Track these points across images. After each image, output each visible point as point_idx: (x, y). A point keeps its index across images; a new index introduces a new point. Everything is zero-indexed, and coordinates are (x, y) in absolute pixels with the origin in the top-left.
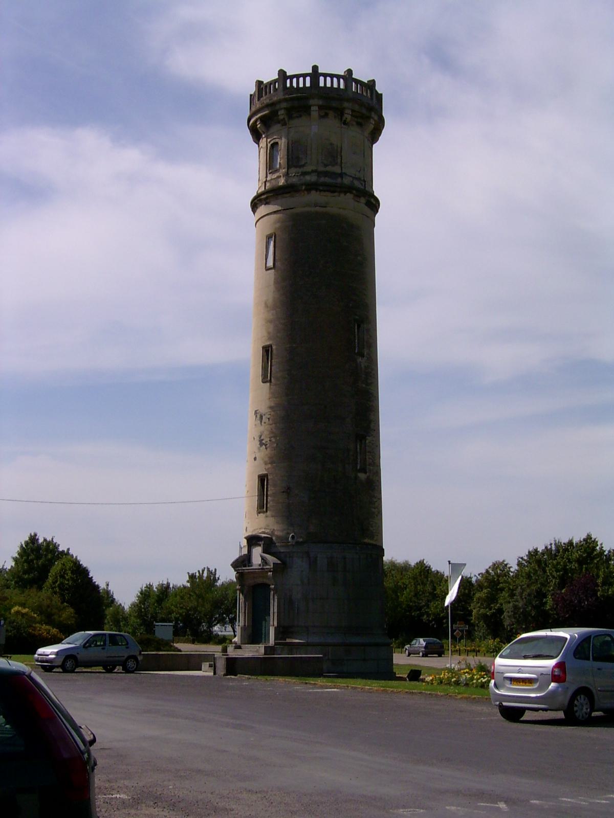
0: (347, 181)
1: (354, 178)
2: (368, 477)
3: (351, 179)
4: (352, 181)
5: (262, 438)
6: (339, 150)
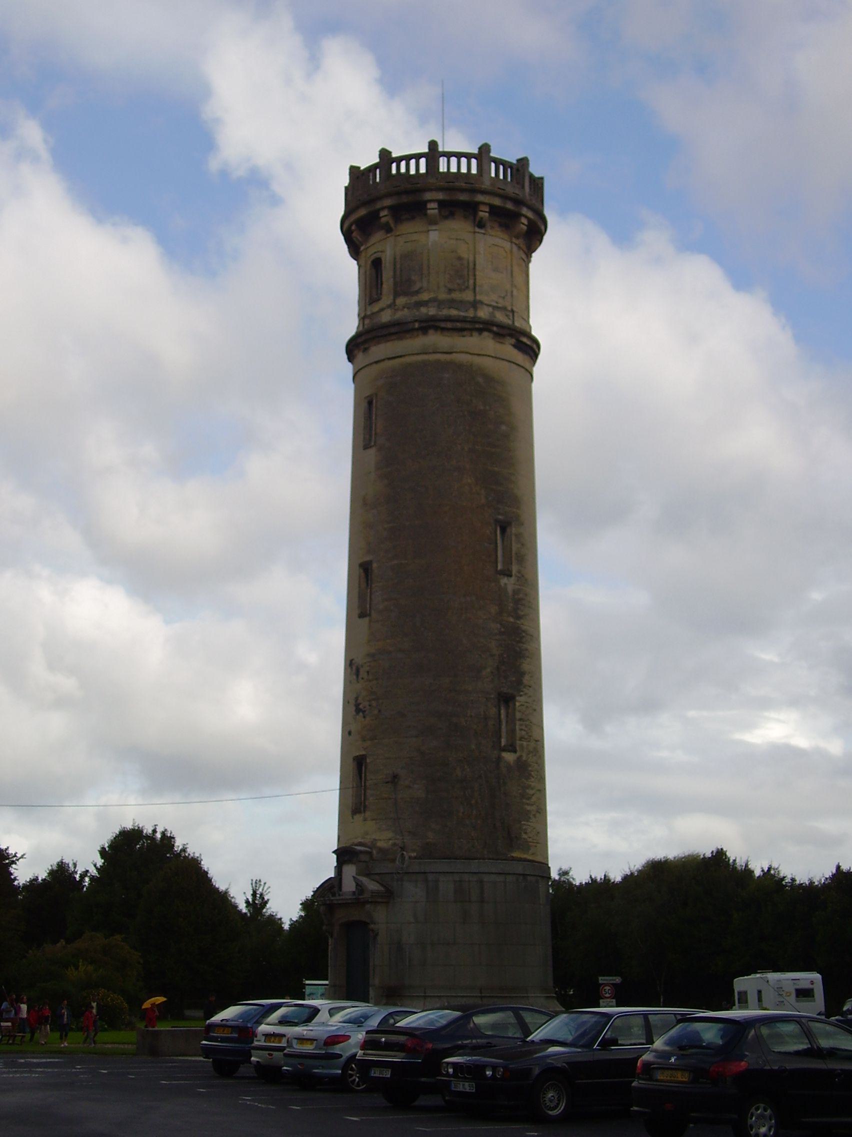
0: (483, 313)
1: (495, 308)
2: (519, 758)
3: (491, 309)
4: (493, 313)
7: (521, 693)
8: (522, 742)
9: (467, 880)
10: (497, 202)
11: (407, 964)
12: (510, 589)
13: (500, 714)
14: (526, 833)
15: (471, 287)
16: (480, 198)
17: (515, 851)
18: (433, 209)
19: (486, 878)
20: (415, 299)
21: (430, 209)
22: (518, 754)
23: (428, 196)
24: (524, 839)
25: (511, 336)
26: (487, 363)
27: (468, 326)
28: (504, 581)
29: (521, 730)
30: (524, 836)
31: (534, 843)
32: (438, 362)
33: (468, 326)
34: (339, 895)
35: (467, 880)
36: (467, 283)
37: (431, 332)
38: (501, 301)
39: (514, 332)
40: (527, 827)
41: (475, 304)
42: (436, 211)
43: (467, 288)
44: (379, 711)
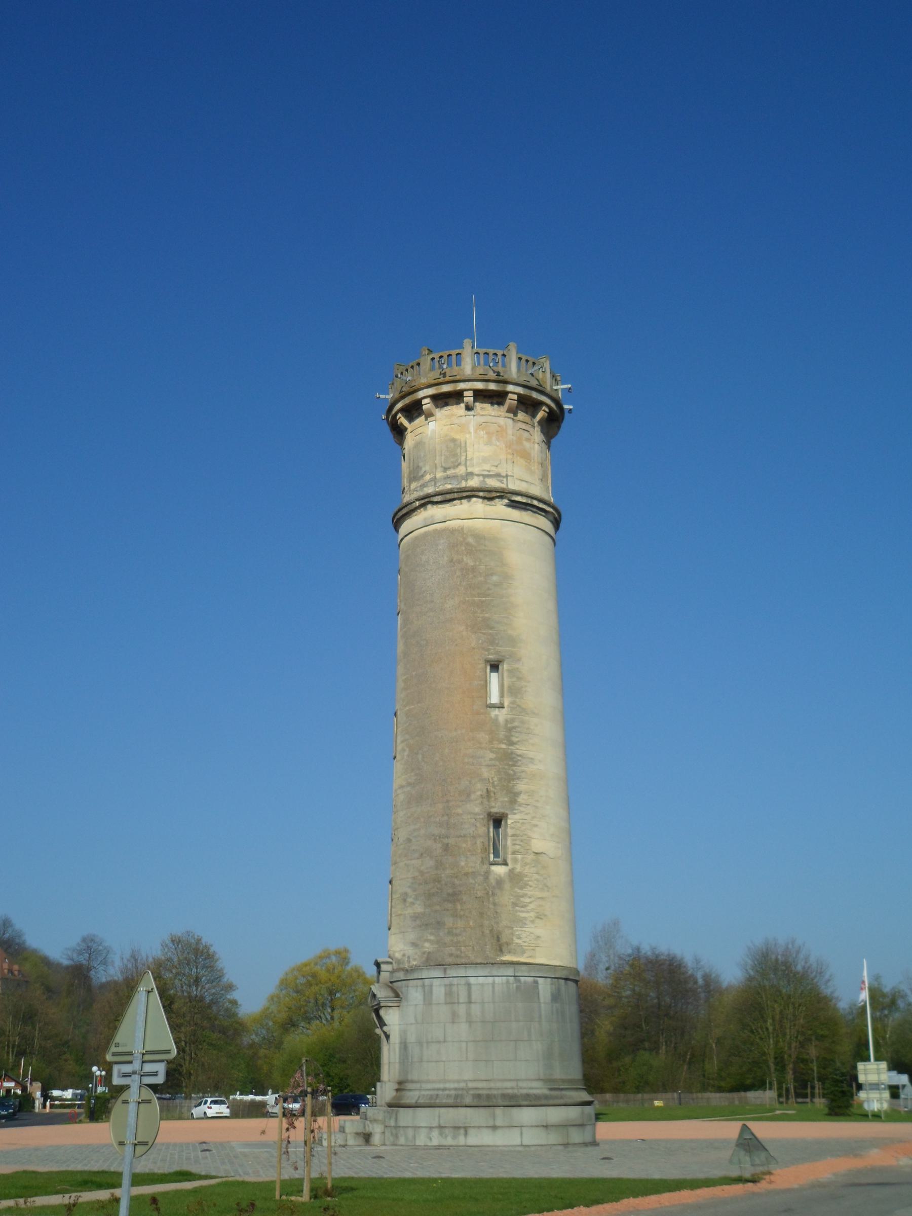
0: (474, 483)
1: (485, 476)
2: (512, 871)
3: (481, 478)
4: (484, 481)
7: (515, 811)
8: (515, 855)
9: (456, 983)
10: (480, 386)
11: (410, 1061)
12: (501, 719)
13: (489, 832)
14: (519, 938)
15: (463, 463)
16: (510, 388)
17: (506, 955)
18: (469, 397)
19: (472, 980)
20: (421, 482)
21: (425, 405)
22: (510, 866)
23: (421, 394)
24: (517, 943)
25: (501, 497)
26: (478, 524)
27: (456, 495)
28: (495, 712)
29: (514, 844)
30: (517, 941)
31: (177, 953)
32: (435, 531)
33: (456, 495)
35: (456, 983)
36: (443, 460)
37: (474, 499)
38: (494, 469)
39: (502, 494)
40: (520, 932)
41: (470, 475)
42: (472, 398)
43: (459, 464)
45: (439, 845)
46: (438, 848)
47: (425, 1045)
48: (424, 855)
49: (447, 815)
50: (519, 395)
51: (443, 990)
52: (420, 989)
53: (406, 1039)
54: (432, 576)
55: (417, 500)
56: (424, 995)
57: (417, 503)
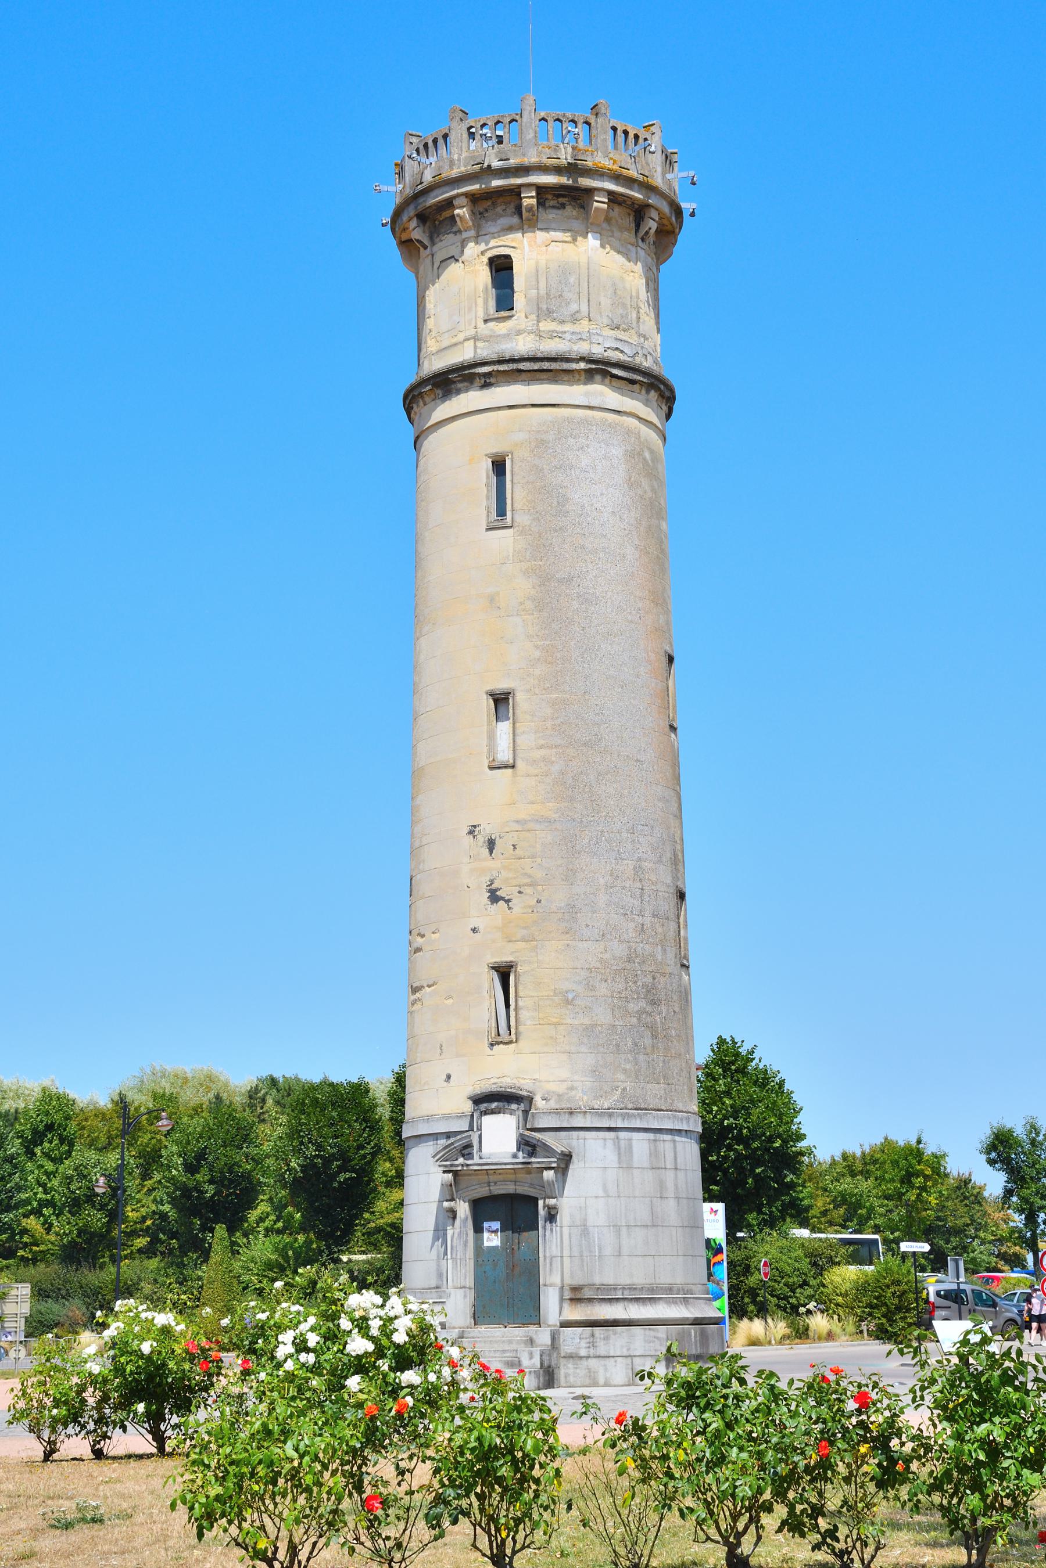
5: (494, 887)
6: (634, 294)
34: (481, 1158)
44: (539, 901)
45: (632, 925)
46: (630, 930)
47: (624, 1230)
48: (609, 936)
49: (641, 880)
50: (610, 193)
51: (646, 1145)
52: (610, 1143)
53: (585, 1220)
54: (602, 494)
55: (582, 359)
56: (619, 1154)
57: (582, 365)
